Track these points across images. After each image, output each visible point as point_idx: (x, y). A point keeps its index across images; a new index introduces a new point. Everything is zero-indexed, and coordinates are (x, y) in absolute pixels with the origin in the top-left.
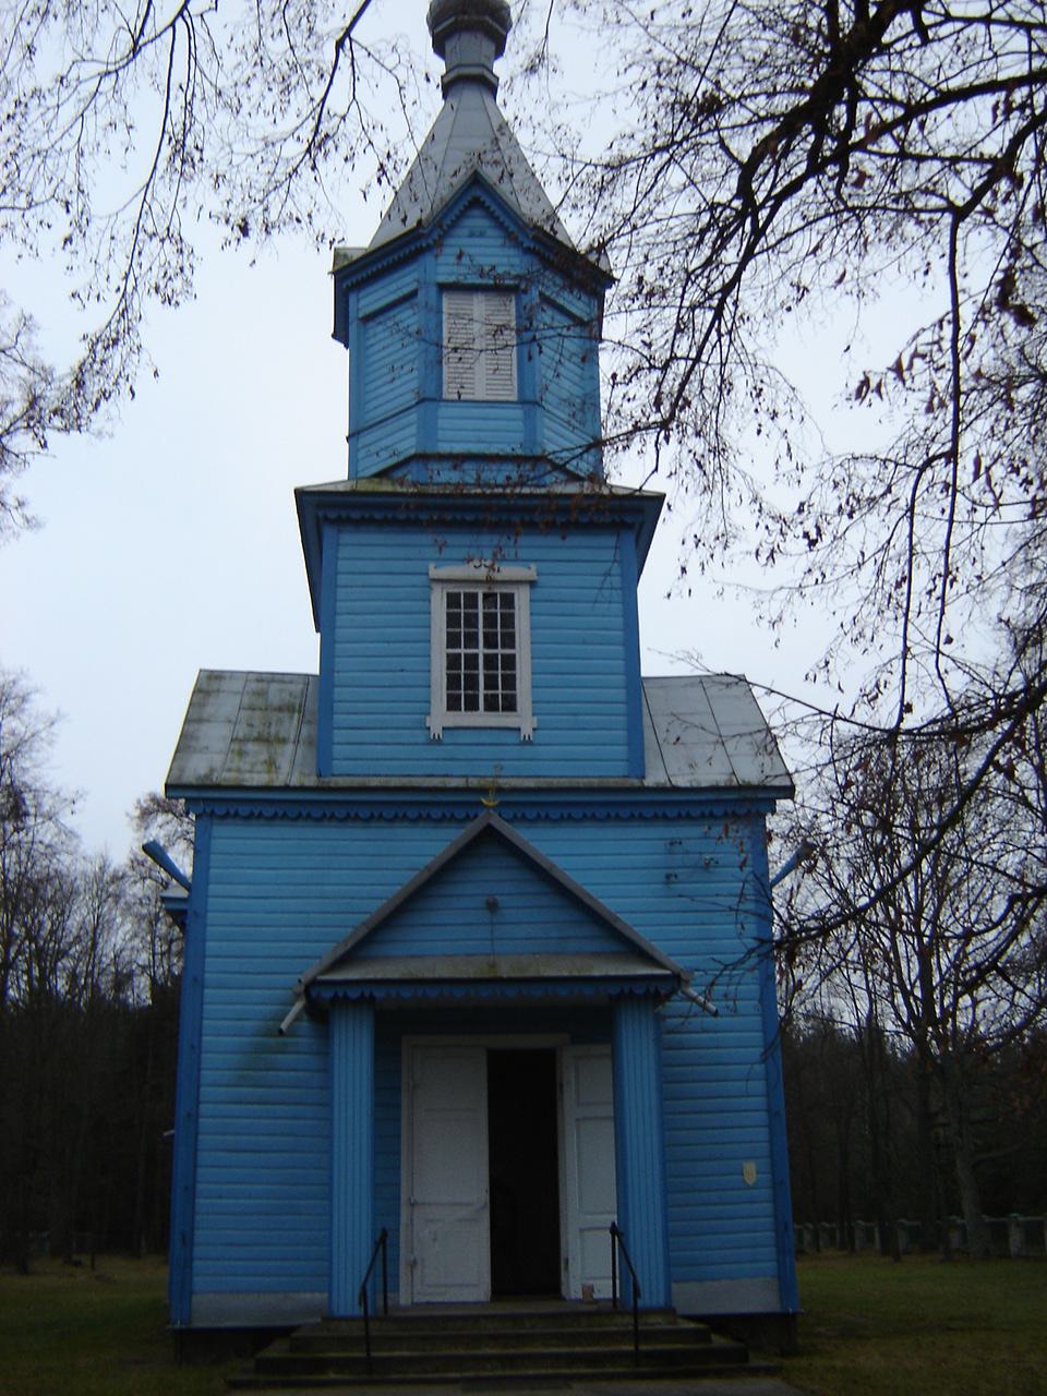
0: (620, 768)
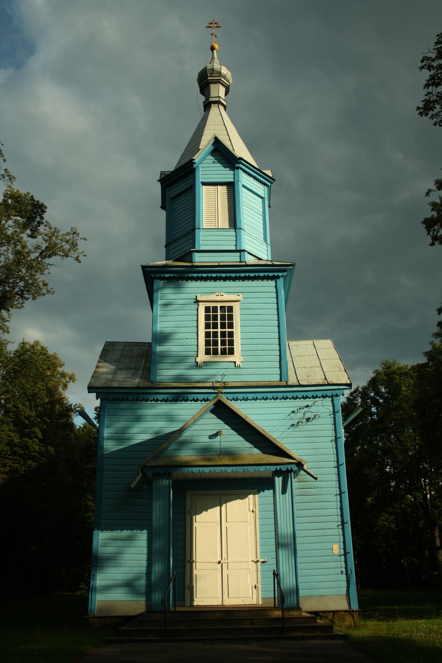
0: (277, 378)
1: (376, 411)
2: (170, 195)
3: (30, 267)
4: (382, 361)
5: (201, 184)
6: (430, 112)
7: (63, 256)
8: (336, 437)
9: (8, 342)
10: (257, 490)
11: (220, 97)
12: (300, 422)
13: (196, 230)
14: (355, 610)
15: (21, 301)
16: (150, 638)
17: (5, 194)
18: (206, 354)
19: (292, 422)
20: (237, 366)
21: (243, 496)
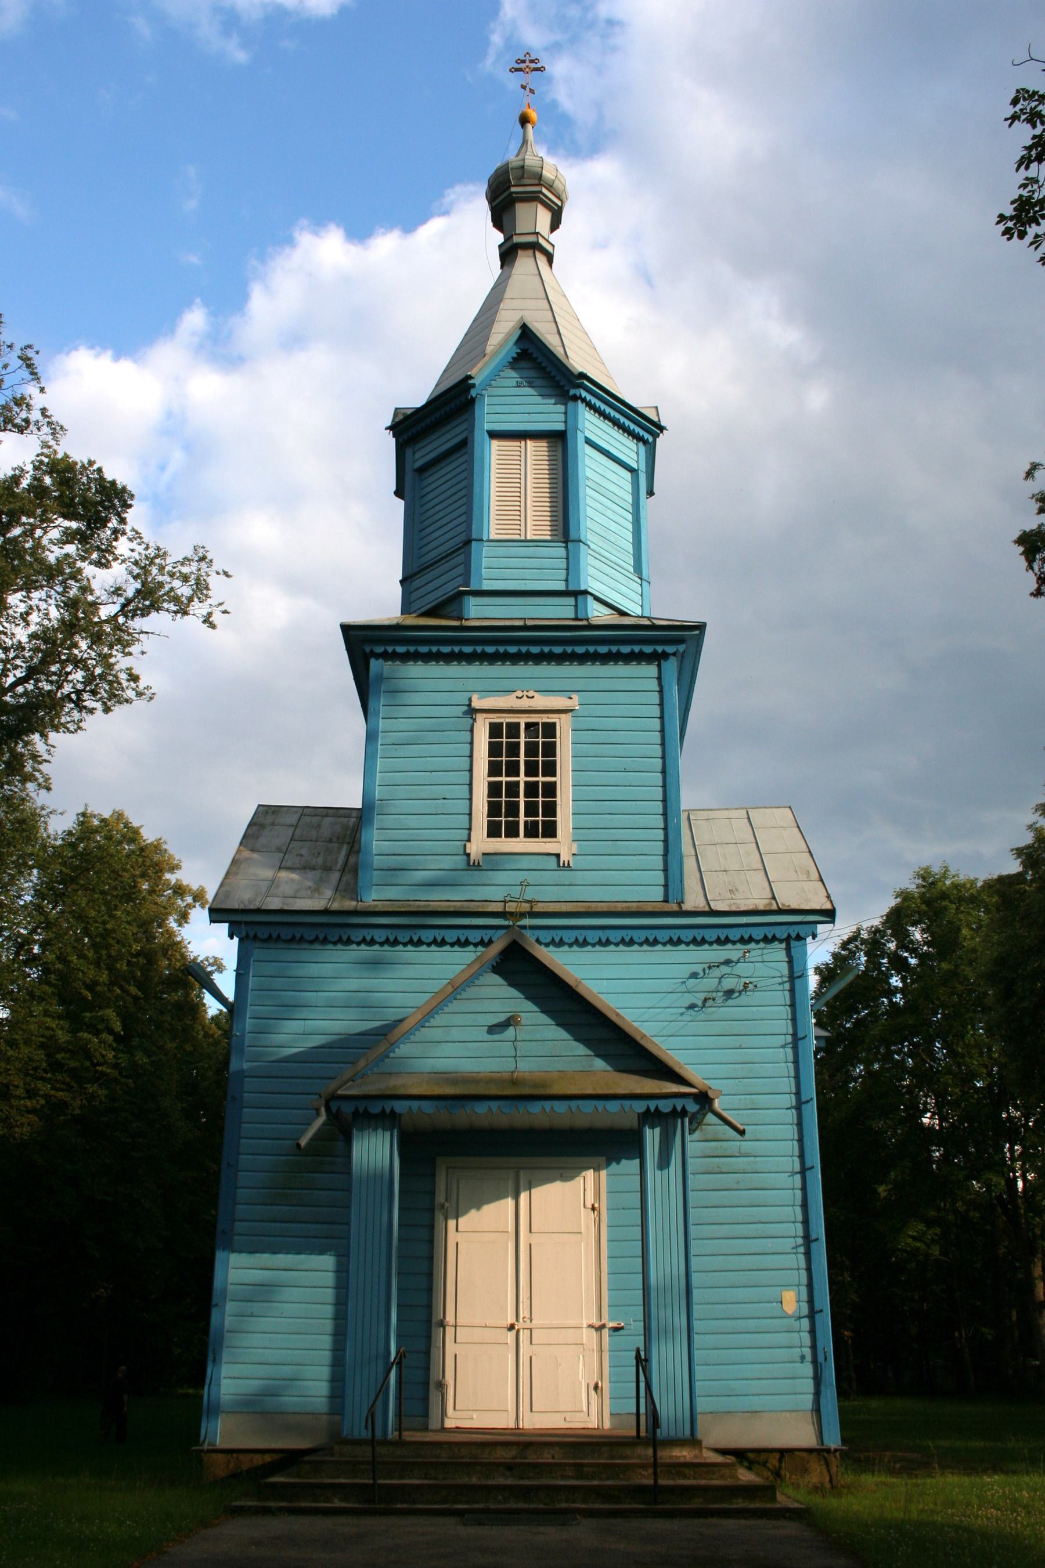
0: (658, 894)
1: (901, 985)
2: (415, 462)
3: (96, 639)
4: (917, 870)
5: (486, 436)
6: (1030, 227)
7: (176, 612)
8: (794, 1035)
9: (51, 813)
10: (604, 1158)
11: (538, 234)
12: (709, 999)
13: (474, 543)
14: (832, 1448)
15: (76, 715)
16: (337, 1503)
17: (37, 464)
18: (489, 836)
19: (689, 999)
20: (564, 864)
21: (567, 1174)
